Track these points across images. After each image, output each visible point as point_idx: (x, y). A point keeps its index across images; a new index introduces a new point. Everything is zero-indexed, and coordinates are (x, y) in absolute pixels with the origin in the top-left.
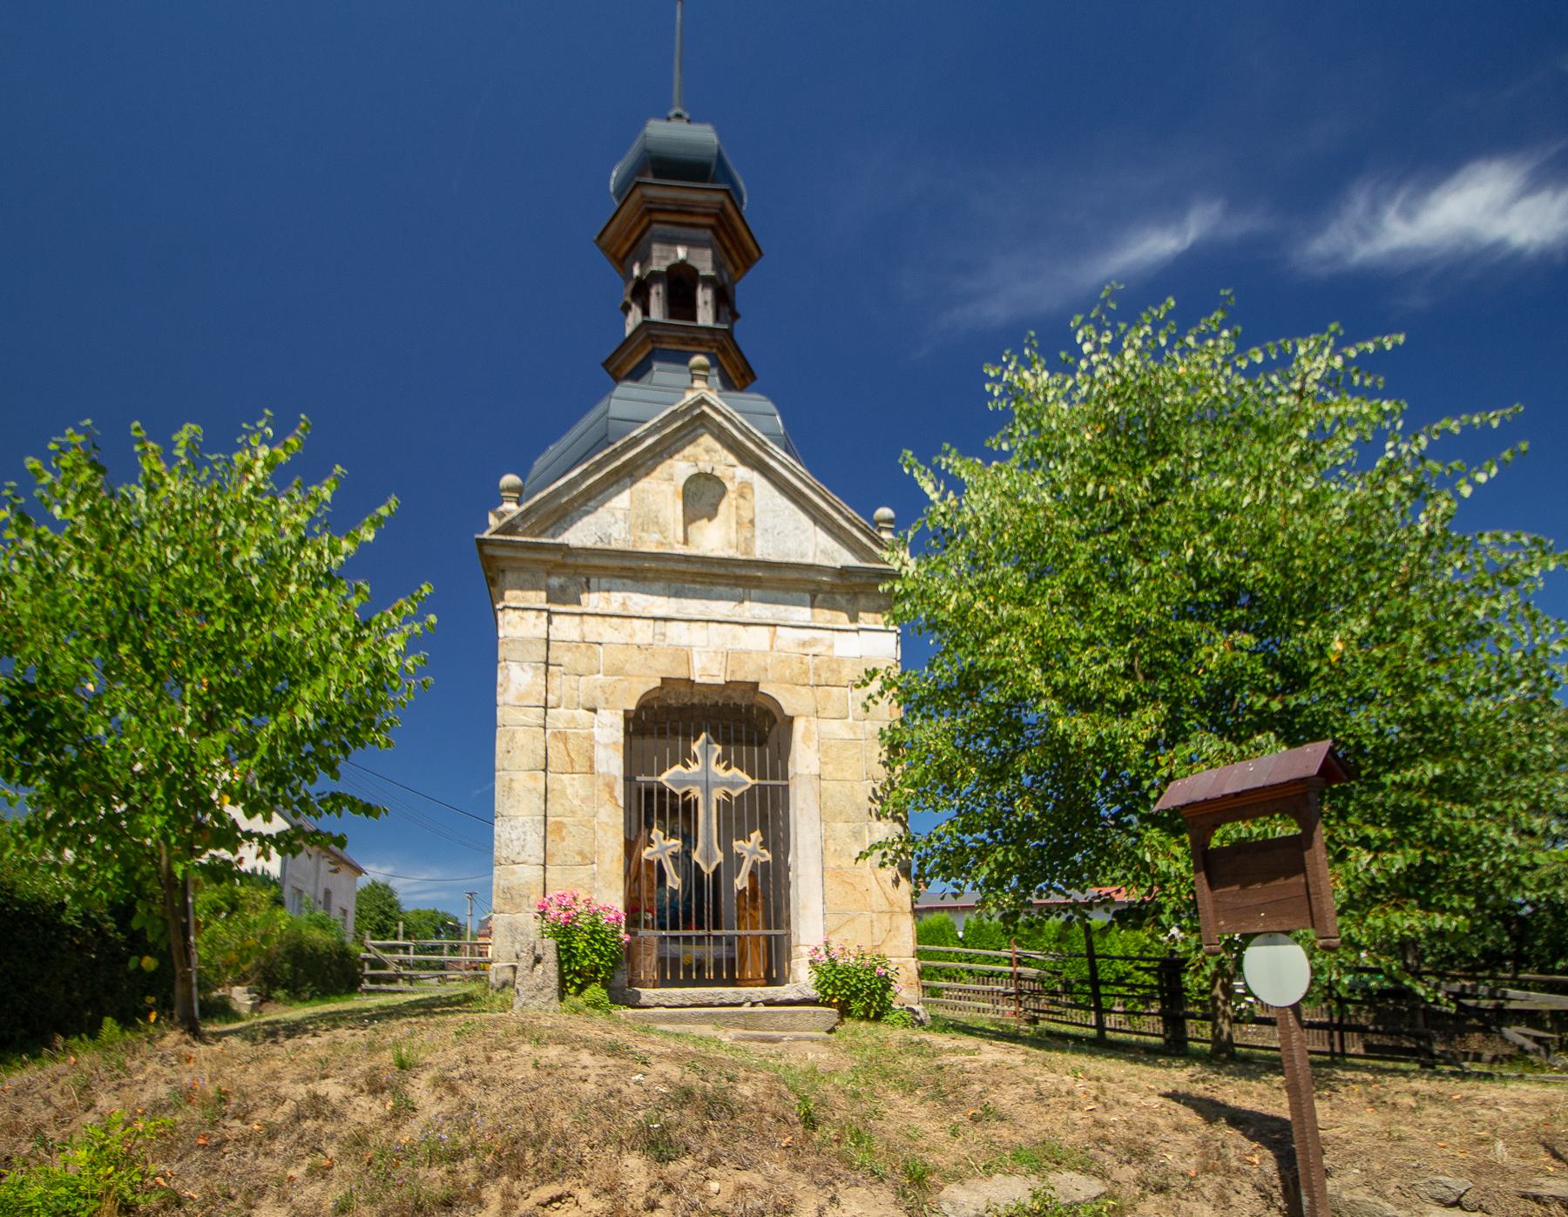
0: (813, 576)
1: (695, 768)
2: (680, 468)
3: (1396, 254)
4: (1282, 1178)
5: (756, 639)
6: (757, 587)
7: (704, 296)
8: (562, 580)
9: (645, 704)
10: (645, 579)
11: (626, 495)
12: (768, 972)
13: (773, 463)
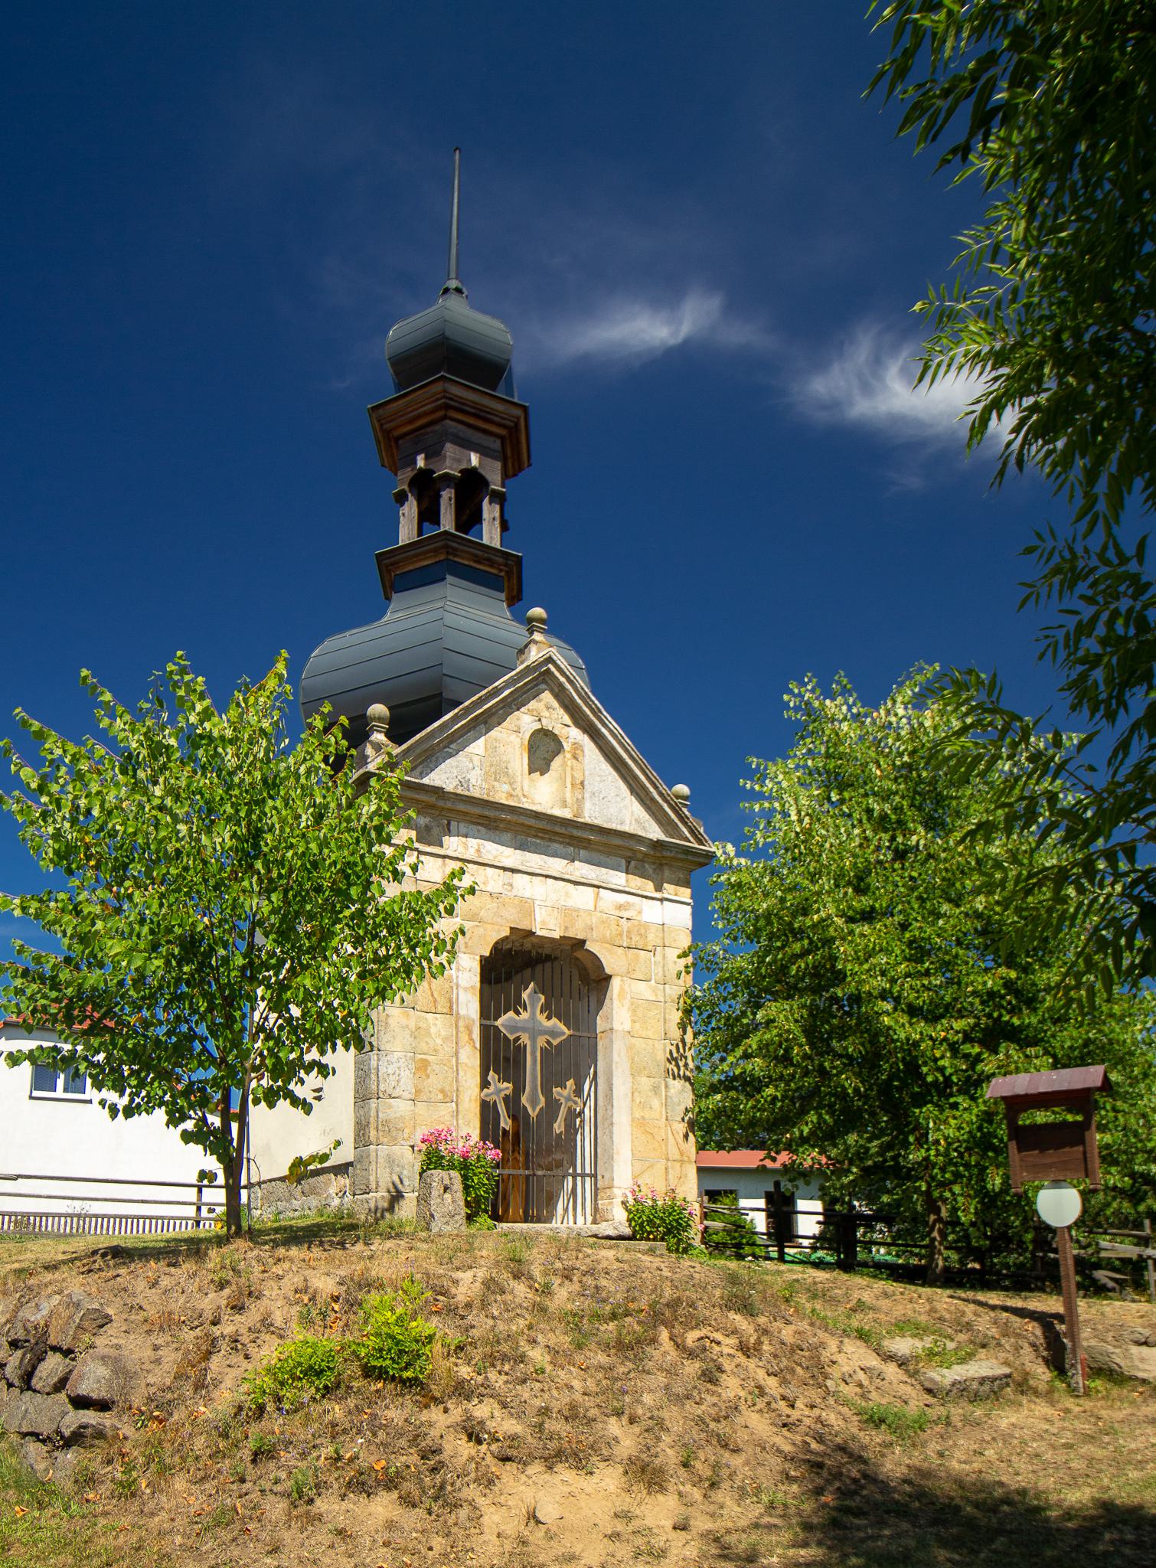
0: (632, 844)
1: (525, 1015)
2: (524, 721)
3: (898, 420)
4: (1046, 1337)
5: (583, 898)
6: (585, 848)
7: (490, 512)
8: (428, 819)
9: (497, 948)
10: (496, 828)
11: (481, 741)
12: (526, 1212)
13: (603, 730)
